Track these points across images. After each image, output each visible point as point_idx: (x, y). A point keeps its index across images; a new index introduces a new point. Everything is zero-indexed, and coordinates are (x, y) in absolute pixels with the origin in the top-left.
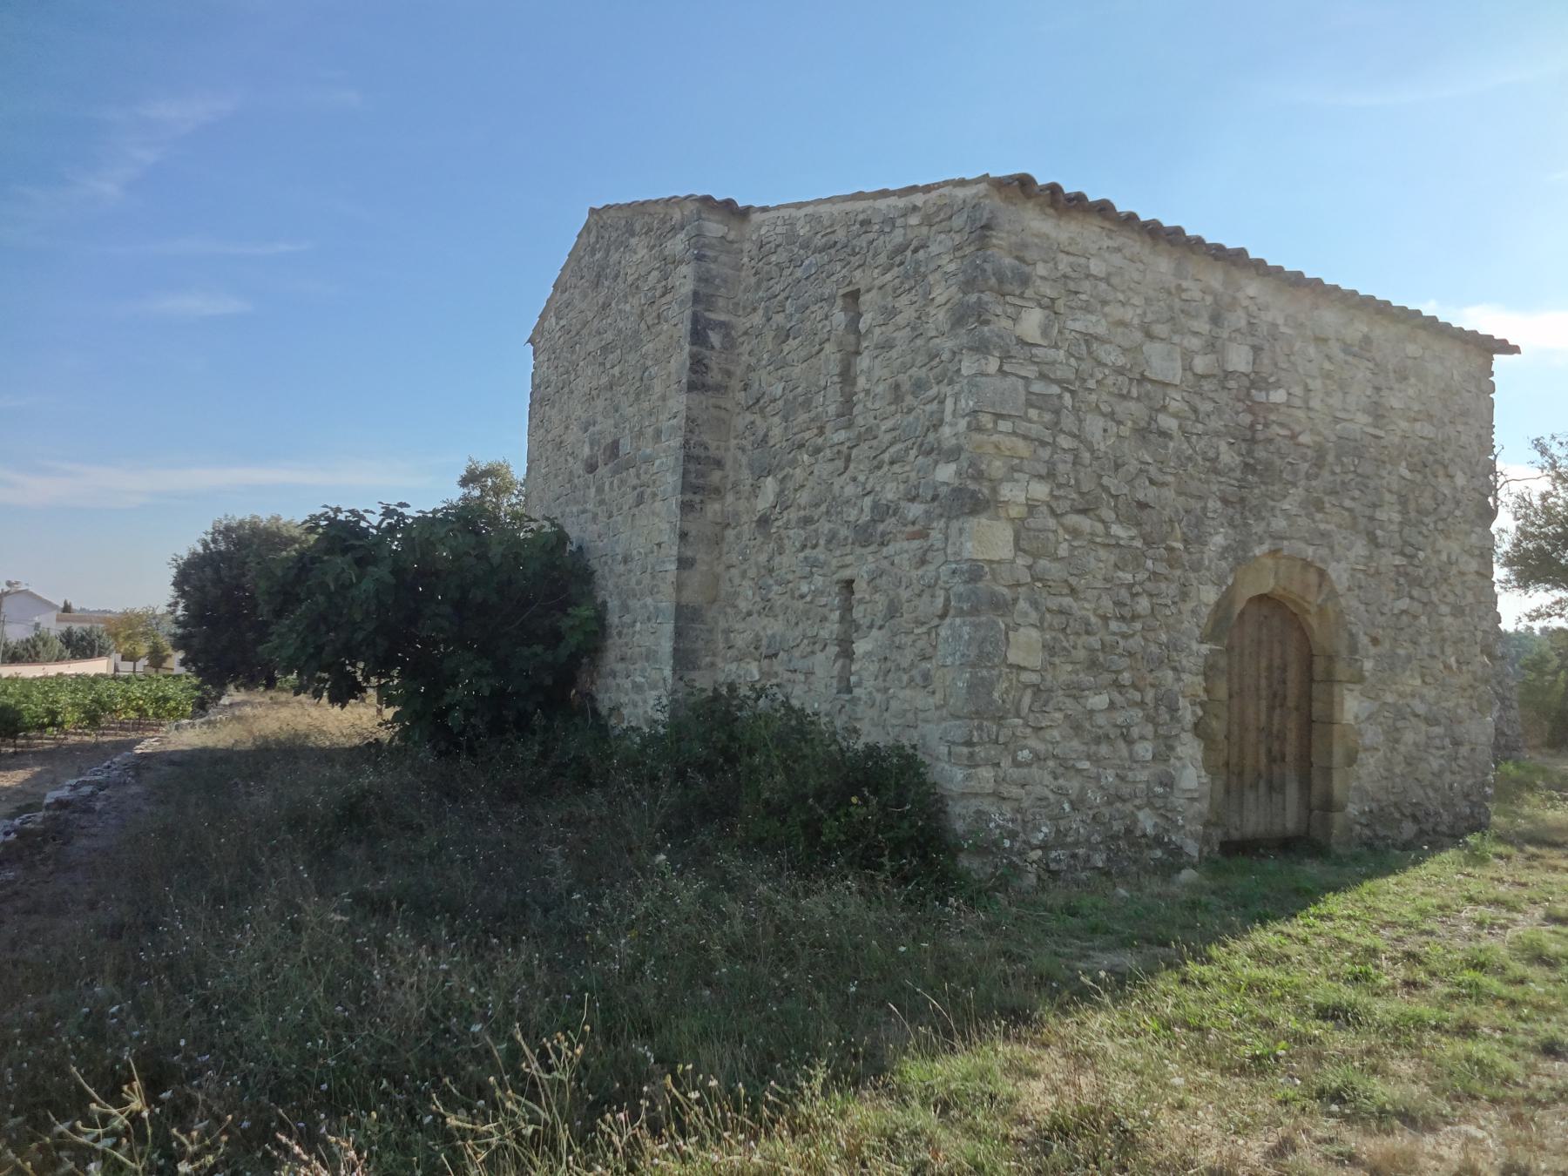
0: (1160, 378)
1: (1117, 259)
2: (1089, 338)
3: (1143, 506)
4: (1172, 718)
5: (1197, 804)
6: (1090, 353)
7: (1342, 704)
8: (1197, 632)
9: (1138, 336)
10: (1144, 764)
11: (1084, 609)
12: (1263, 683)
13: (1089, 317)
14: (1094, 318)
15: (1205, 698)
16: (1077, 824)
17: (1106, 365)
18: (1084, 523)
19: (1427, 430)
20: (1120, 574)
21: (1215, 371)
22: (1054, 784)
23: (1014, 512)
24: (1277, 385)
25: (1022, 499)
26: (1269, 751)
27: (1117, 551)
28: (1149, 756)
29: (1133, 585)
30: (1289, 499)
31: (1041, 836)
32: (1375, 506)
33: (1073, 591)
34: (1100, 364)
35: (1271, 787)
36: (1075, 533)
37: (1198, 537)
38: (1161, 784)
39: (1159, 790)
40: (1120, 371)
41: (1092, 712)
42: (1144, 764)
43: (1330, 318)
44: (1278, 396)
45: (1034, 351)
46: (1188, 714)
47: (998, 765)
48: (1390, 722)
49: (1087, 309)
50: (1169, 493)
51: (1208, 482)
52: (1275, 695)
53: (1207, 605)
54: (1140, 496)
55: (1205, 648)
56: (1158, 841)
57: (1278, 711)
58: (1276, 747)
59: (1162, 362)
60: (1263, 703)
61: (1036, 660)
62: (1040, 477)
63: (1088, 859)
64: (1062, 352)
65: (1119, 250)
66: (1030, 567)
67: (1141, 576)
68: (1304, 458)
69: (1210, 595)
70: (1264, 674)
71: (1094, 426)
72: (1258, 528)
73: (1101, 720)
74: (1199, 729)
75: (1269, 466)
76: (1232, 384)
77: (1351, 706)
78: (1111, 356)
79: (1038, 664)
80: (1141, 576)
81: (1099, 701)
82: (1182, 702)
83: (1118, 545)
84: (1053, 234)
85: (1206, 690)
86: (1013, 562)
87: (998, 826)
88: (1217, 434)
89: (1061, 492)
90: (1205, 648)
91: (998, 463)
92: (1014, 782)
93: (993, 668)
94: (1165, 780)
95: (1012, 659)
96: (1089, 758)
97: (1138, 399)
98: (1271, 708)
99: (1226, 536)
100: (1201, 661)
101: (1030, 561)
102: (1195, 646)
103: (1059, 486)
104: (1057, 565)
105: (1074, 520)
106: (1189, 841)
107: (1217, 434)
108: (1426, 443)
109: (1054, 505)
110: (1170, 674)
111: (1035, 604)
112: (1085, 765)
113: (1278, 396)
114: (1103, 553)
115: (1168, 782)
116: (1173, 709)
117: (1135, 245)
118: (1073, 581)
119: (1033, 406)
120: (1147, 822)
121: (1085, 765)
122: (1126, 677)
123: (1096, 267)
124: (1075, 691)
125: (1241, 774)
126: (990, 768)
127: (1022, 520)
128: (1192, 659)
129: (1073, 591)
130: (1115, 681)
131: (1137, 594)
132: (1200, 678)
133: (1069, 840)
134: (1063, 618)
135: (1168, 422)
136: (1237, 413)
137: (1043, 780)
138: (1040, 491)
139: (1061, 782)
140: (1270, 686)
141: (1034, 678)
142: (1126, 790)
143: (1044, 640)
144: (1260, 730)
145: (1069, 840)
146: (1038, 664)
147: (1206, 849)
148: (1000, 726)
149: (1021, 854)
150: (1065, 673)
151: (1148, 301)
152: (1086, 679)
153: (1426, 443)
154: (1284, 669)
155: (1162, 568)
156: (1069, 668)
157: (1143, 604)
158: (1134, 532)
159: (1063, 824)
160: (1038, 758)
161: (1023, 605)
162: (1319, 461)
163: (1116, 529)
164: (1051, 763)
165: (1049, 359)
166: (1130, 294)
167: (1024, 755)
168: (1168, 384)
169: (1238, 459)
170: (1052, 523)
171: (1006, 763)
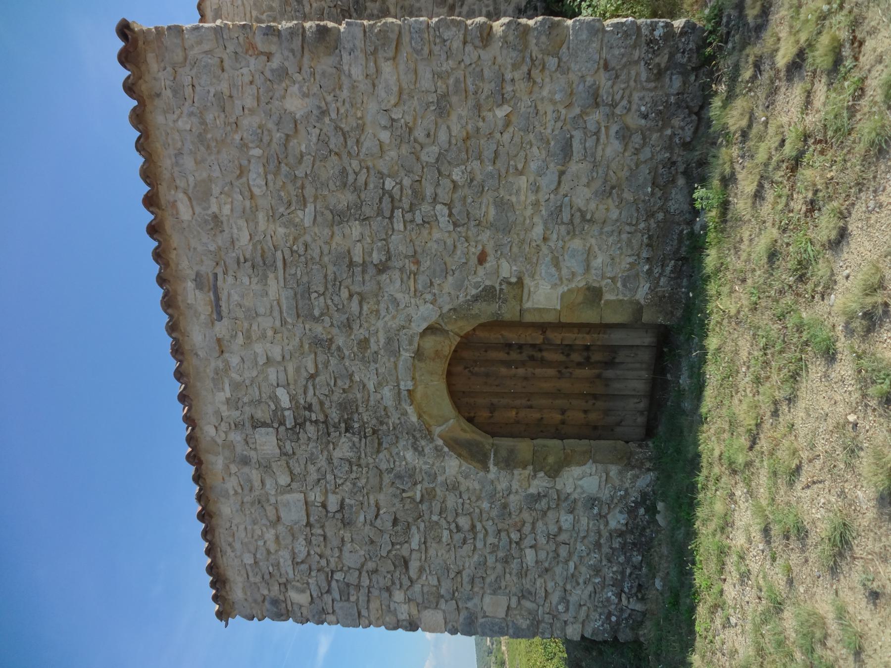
0: (304, 513)
1: (237, 545)
2: (295, 564)
3: (395, 522)
4: (545, 496)
5: (612, 474)
6: (302, 562)
7: (539, 310)
8: (481, 474)
9: (281, 528)
10: (576, 521)
11: (470, 565)
12: (521, 371)
13: (282, 564)
14: (282, 560)
15: (530, 468)
16: (610, 572)
17: (308, 552)
18: (414, 565)
19: (256, 179)
20: (444, 539)
21: (284, 463)
22: (582, 585)
23: (414, 612)
24: (274, 398)
25: (406, 606)
26: (579, 365)
27: (428, 544)
28: (570, 517)
29: (451, 531)
30: (366, 381)
31: (613, 597)
32: (351, 264)
33: (459, 573)
34: (309, 554)
35: (610, 364)
36: (421, 570)
37: (411, 476)
38: (592, 508)
39: (596, 510)
40: (309, 542)
41: (537, 562)
42: (576, 521)
43: (198, 336)
44: (285, 401)
45: (315, 596)
46: (540, 483)
47: (565, 622)
48: (563, 228)
49: (277, 565)
50: (382, 497)
51: (367, 466)
52: (532, 358)
53: (460, 466)
54: (389, 524)
55: (493, 468)
56: (631, 512)
57: (546, 355)
58: (576, 357)
59: (293, 508)
60: (538, 371)
61: (503, 600)
62: (390, 596)
63: (635, 567)
64: (310, 580)
65: (230, 545)
66: (446, 601)
67: (443, 523)
68: (326, 364)
69: (453, 465)
70: (513, 371)
71: (351, 560)
72: (394, 419)
73: (542, 555)
74: (554, 473)
75: (343, 406)
76: (288, 448)
77: (545, 296)
78: (301, 548)
79: (506, 598)
80: (443, 523)
81: (530, 556)
82: (533, 490)
83: (425, 543)
84: (240, 585)
85: (525, 468)
86: (444, 611)
87: (602, 626)
88: (330, 460)
89: (397, 582)
90: (493, 468)
91: (387, 619)
92: (578, 612)
93: (507, 626)
94: (590, 505)
95: (503, 615)
96: (567, 562)
97: (323, 527)
98: (543, 363)
99: (405, 448)
100: (503, 473)
101: (442, 601)
102: (491, 476)
103: (393, 583)
104: (443, 584)
105: (413, 573)
106: (638, 484)
107: (330, 460)
108: (270, 177)
109: (405, 587)
110: (512, 497)
111: (469, 599)
112: (571, 565)
113: (285, 401)
114: (432, 552)
115: (592, 501)
116: (538, 497)
117: (222, 537)
118: (452, 575)
119: (349, 598)
120: (617, 520)
121: (571, 565)
122: (515, 536)
123: (249, 560)
124: (523, 573)
125: (595, 397)
126: (567, 627)
127: (418, 605)
128: (501, 479)
129: (459, 573)
130: (517, 543)
131: (457, 526)
132: (516, 472)
133: (619, 578)
134: (477, 580)
135: (333, 503)
136: (309, 439)
137: (579, 594)
138: (399, 596)
139: (581, 581)
140: (523, 364)
141: (514, 600)
142: (593, 537)
143: (491, 594)
144: (561, 375)
145: (619, 578)
146: (506, 598)
147: (648, 465)
148: (543, 621)
149: (622, 611)
150: (510, 580)
151: (255, 522)
152: (515, 565)
153: (270, 177)
154: (509, 346)
155: (436, 507)
156: (508, 576)
157: (464, 522)
158: (414, 529)
159: (608, 582)
160: (564, 599)
161: (470, 605)
162: (321, 344)
163: (415, 545)
164: (568, 587)
165: (317, 588)
166: (256, 537)
167: (561, 608)
168: (306, 503)
169: (343, 440)
170: (417, 588)
171: (565, 617)
